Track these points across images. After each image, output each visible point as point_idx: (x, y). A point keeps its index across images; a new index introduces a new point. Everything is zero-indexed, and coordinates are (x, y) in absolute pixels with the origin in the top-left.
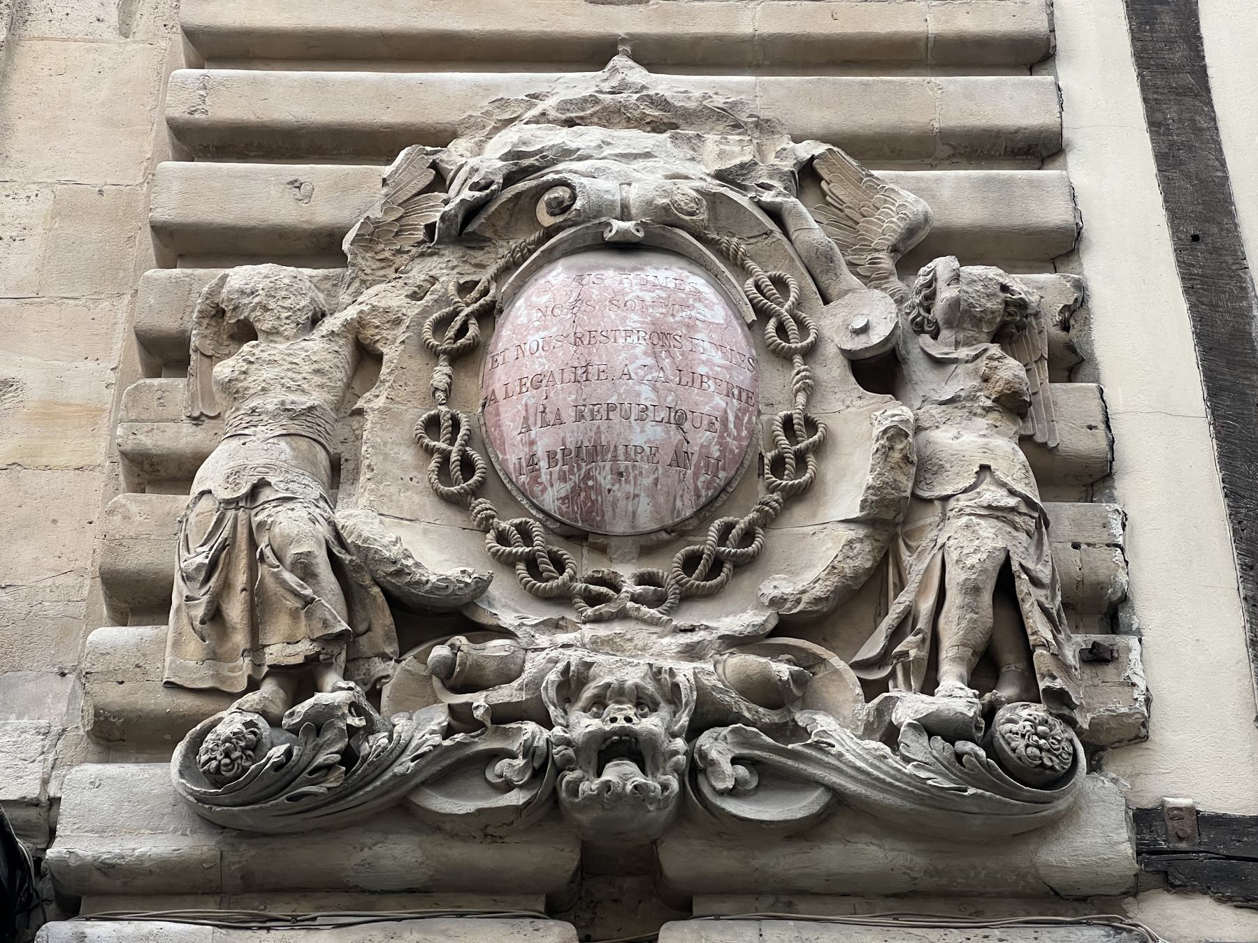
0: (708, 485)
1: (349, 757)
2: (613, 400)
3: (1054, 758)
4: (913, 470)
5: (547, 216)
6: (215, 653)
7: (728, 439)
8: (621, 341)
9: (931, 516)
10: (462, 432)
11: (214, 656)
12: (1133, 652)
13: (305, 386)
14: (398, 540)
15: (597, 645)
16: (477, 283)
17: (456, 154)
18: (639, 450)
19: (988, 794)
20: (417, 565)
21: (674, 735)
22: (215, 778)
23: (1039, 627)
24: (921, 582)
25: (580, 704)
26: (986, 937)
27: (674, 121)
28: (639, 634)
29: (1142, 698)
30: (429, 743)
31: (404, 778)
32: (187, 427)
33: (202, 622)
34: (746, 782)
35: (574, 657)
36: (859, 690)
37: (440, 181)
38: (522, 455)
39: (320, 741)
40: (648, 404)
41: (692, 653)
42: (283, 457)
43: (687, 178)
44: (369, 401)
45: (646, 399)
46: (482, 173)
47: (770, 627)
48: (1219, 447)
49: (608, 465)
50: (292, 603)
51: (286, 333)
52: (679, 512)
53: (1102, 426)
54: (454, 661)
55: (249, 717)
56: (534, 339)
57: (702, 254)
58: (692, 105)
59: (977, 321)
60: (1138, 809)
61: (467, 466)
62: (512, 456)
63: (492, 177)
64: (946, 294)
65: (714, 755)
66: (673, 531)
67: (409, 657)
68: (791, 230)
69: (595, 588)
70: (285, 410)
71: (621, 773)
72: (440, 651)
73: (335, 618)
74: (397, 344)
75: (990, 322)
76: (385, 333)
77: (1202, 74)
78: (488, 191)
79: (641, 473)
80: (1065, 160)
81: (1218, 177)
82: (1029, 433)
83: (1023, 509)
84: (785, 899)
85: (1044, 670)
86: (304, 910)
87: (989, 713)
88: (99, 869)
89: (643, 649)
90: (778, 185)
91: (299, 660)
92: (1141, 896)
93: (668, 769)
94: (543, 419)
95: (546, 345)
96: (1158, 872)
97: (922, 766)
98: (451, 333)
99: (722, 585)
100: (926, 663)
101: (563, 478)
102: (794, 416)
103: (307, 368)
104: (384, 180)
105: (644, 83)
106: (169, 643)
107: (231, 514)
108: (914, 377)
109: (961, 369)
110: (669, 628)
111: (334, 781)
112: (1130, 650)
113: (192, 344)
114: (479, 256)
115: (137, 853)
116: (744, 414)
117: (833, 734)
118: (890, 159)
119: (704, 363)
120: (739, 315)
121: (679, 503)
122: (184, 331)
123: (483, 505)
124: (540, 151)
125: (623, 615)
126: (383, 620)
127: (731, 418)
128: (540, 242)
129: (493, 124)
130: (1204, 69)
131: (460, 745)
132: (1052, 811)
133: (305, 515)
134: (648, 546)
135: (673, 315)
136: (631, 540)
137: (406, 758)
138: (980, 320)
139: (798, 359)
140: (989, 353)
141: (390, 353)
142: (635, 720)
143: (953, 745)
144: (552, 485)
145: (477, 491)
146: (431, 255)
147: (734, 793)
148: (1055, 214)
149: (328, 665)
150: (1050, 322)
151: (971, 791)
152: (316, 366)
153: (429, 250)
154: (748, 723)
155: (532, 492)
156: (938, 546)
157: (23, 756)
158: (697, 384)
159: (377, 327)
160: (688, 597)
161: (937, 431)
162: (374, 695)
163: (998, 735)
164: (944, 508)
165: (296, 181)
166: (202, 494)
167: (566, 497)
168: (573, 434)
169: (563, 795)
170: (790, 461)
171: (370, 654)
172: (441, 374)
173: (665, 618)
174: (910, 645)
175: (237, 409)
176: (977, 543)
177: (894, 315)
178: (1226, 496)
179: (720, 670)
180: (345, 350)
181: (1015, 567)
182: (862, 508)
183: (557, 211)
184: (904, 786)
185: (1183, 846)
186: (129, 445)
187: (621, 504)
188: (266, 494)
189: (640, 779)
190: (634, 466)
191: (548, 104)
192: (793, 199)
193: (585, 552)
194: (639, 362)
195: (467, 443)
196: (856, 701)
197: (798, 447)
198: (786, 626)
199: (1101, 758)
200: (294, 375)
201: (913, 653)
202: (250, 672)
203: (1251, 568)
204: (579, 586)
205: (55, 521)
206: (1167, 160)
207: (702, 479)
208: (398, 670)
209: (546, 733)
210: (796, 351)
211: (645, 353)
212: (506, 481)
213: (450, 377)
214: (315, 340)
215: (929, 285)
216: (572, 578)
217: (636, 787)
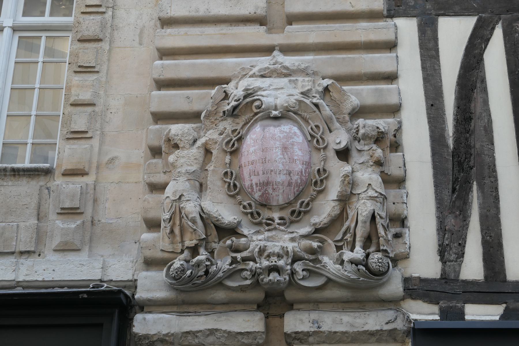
0: (297, 191)
1: (207, 272)
2: (272, 169)
3: (383, 268)
4: (351, 186)
5: (255, 109)
6: (172, 242)
7: (303, 177)
8: (274, 151)
9: (354, 199)
10: (234, 177)
11: (172, 243)
12: (407, 234)
13: (192, 164)
14: (217, 211)
15: (267, 239)
16: (237, 130)
17: (230, 87)
18: (279, 183)
19: (365, 279)
20: (222, 218)
21: (287, 265)
22: (174, 278)
23: (381, 231)
24: (352, 219)
25: (264, 256)
26: (365, 314)
27: (290, 73)
28: (280, 234)
29: (408, 247)
30: (226, 268)
31: (220, 278)
32: (162, 175)
33: (169, 234)
34: (306, 276)
35: (262, 243)
36: (335, 249)
37: (226, 96)
38: (249, 184)
39: (199, 269)
40: (281, 169)
41: (293, 240)
42: (187, 187)
43: (293, 95)
44: (209, 167)
45: (281, 168)
46: (237, 96)
47: (313, 232)
48: (434, 171)
49: (271, 187)
50: (191, 230)
51: (187, 148)
52: (290, 199)
53: (403, 167)
54: (232, 244)
55: (182, 263)
56: (252, 149)
57: (297, 119)
58: (295, 68)
59: (370, 138)
60: (405, 278)
61: (235, 186)
62: (247, 183)
63: (240, 97)
64: (362, 131)
65: (297, 270)
66: (288, 203)
67: (221, 242)
68: (321, 110)
69: (268, 222)
70: (187, 172)
71: (274, 277)
72: (229, 242)
73: (202, 234)
74: (216, 150)
75: (374, 138)
76: (213, 146)
77: (437, 51)
78: (239, 102)
79: (280, 189)
80: (398, 81)
81: (439, 85)
82: (383, 170)
83: (380, 196)
84: (317, 304)
85: (382, 244)
86: (198, 309)
87: (367, 256)
88: (148, 300)
89: (280, 239)
90: (318, 96)
91: (193, 245)
92: (405, 300)
93: (286, 274)
94: (254, 174)
95: (255, 152)
96: (409, 295)
97: (349, 272)
98: (230, 146)
99: (301, 219)
100: (352, 241)
101: (260, 191)
102: (321, 169)
103: (193, 158)
104: (211, 97)
105: (282, 61)
106: (161, 238)
107: (174, 204)
108: (353, 156)
109: (365, 153)
110: (287, 232)
111: (203, 279)
112: (406, 233)
113: (163, 150)
114: (237, 120)
115: (156, 296)
116: (307, 169)
117: (328, 263)
118: (350, 81)
119: (296, 155)
120: (306, 138)
121: (290, 197)
122: (160, 146)
123: (239, 198)
124: (253, 88)
125: (275, 229)
126: (214, 232)
127: (303, 171)
128: (254, 116)
129: (241, 76)
130: (438, 49)
131: (234, 268)
132: (382, 282)
133: (193, 205)
134: (282, 208)
135: (288, 141)
136: (277, 207)
137: (221, 272)
138: (371, 138)
139: (322, 150)
140: (373, 148)
141: (214, 152)
142: (277, 262)
143: (357, 266)
144: (257, 192)
145: (237, 194)
146: (225, 120)
147: (304, 278)
148: (393, 100)
149: (201, 246)
150: (391, 137)
151: (361, 279)
152: (195, 157)
153: (224, 119)
154: (306, 260)
155: (252, 194)
156: (356, 209)
157: (127, 268)
158: (294, 161)
159: (211, 144)
160: (292, 222)
161: (358, 173)
162: (212, 253)
163: (369, 263)
164: (358, 197)
165: (188, 97)
166: (167, 197)
167: (261, 196)
168: (262, 178)
169: (260, 281)
170: (319, 182)
171: (211, 241)
172: (228, 159)
173: (286, 230)
174: (348, 237)
175: (175, 171)
176: (366, 208)
177: (347, 139)
178: (434, 186)
179: (299, 245)
180: (202, 151)
181: (376, 214)
182: (337, 197)
183: (257, 108)
184: (345, 278)
185: (416, 287)
186: (148, 181)
187: (275, 198)
188: (183, 198)
189: (279, 278)
190: (278, 187)
191: (255, 70)
192: (322, 101)
193: (266, 209)
194: (279, 157)
195: (235, 180)
196: (334, 252)
197: (321, 178)
198: (317, 231)
199: (397, 263)
200: (189, 161)
201: (349, 239)
202: (181, 248)
203: (439, 208)
204: (264, 221)
205: (131, 199)
206: (426, 80)
207: (296, 189)
208: (219, 246)
209: (255, 265)
210: (321, 148)
211: (280, 154)
212: (245, 190)
213: (230, 160)
214: (194, 149)
215: (357, 128)
216: (262, 219)
217: (277, 280)
